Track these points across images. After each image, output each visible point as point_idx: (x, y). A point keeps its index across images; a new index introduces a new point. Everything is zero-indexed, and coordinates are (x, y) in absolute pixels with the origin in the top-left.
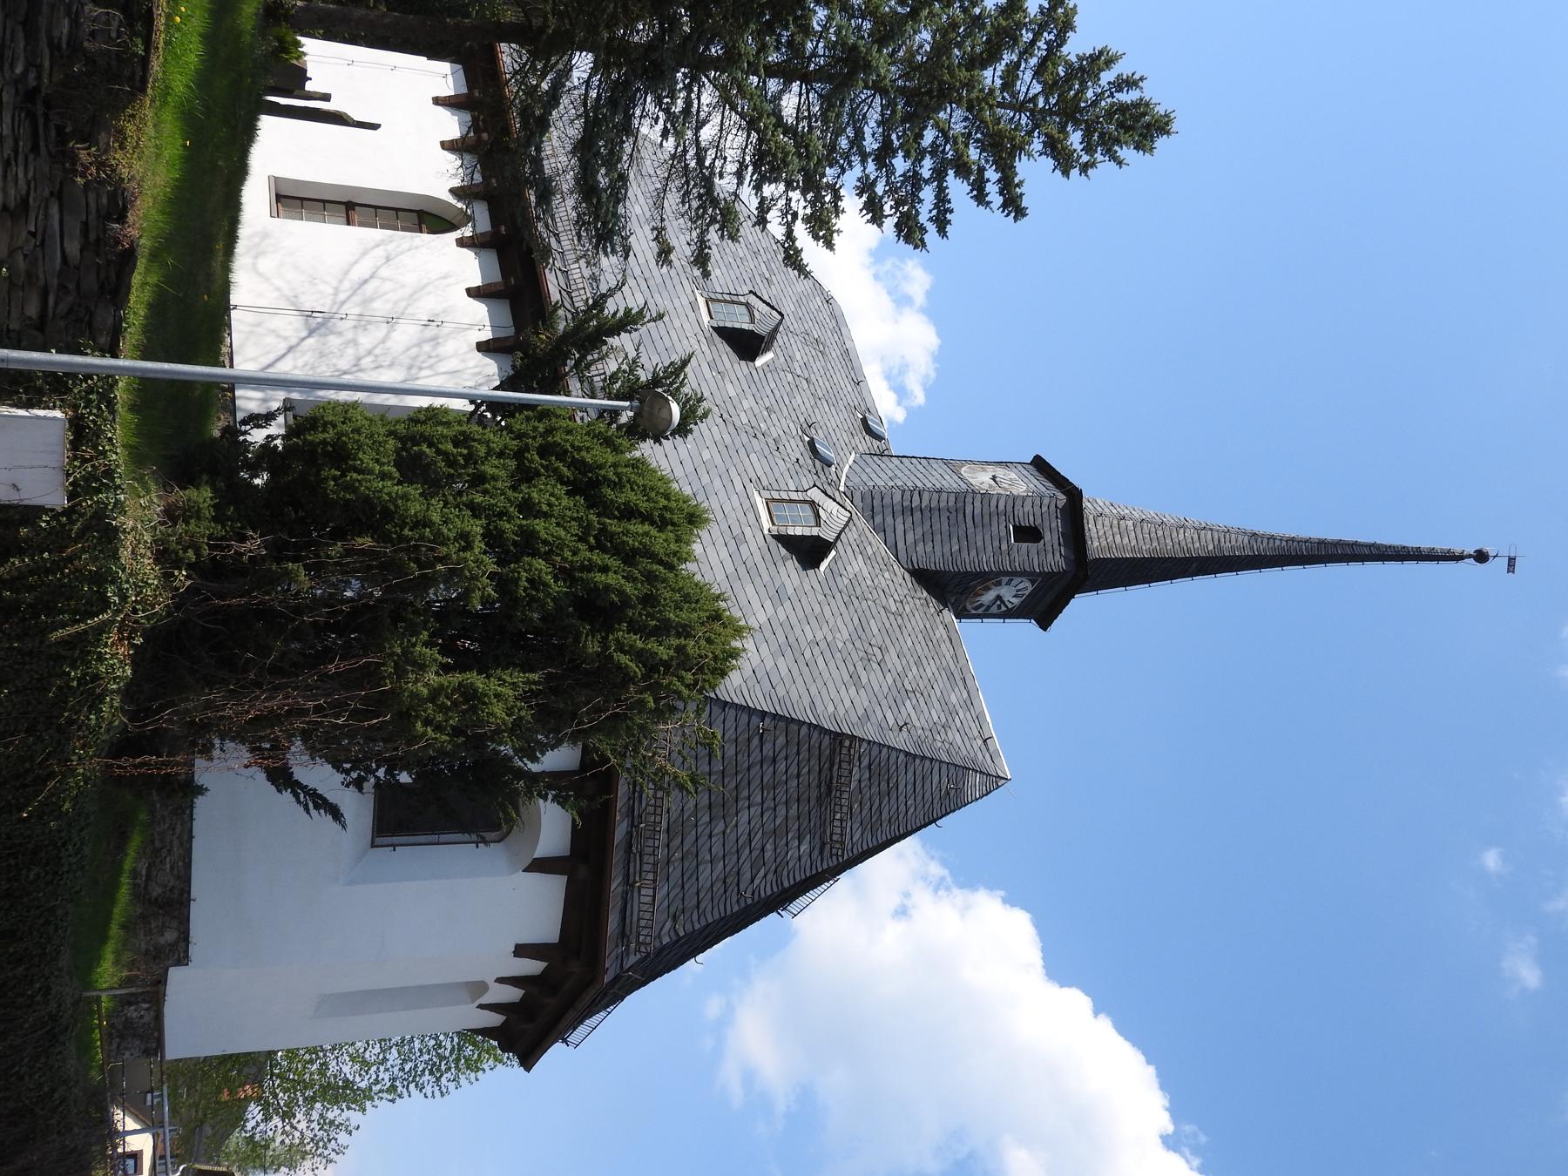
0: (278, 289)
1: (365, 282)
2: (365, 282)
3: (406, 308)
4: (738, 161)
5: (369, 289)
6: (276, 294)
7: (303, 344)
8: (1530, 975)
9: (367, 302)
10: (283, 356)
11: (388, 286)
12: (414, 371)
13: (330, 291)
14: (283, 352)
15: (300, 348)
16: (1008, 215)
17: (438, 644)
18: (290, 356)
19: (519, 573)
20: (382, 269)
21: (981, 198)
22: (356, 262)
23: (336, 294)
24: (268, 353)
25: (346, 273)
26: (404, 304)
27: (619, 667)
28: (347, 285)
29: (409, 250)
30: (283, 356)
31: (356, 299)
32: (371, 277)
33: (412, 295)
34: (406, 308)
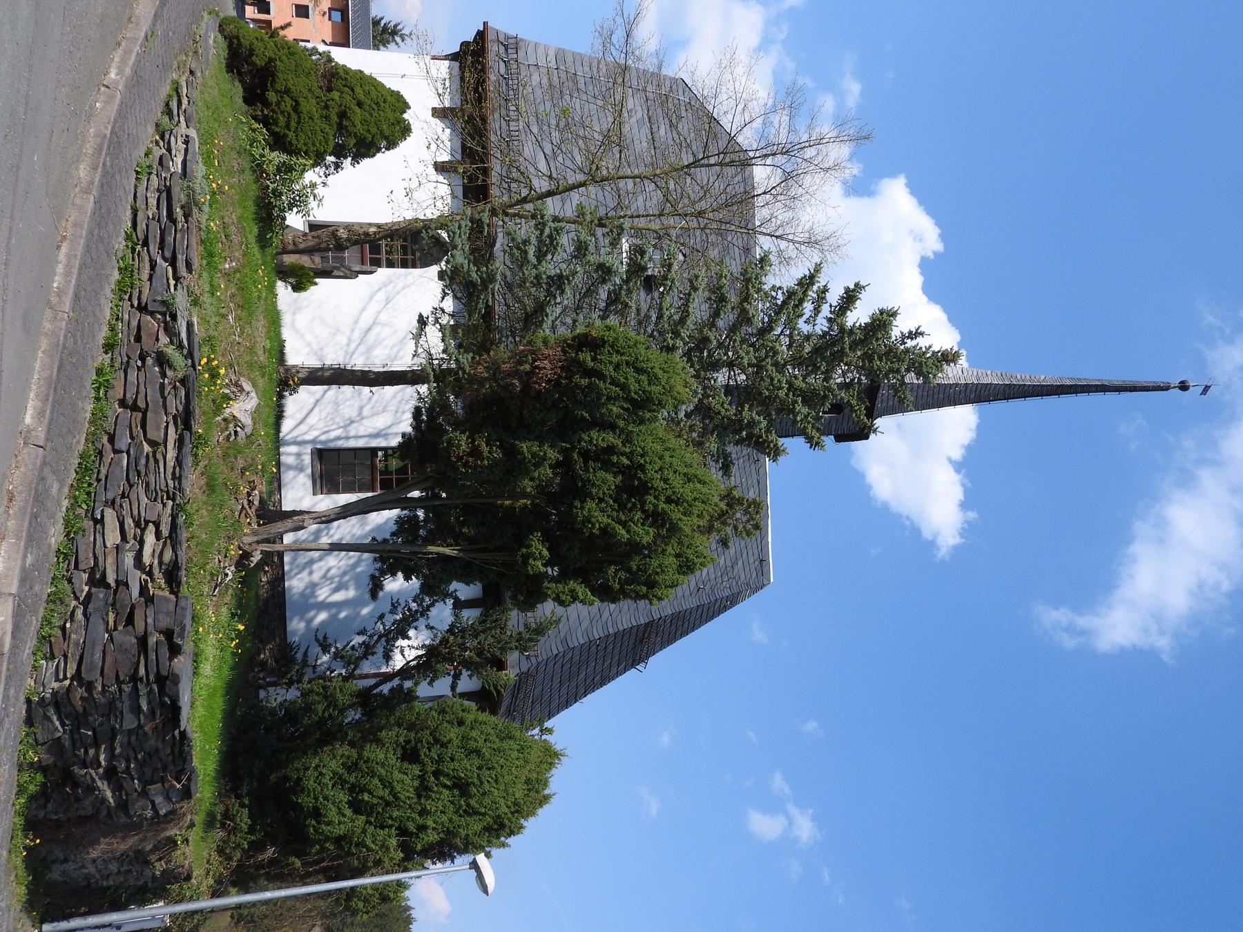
0: (309, 345)
1: (369, 329)
2: (369, 329)
3: (398, 352)
4: (419, 777)
5: (372, 337)
6: (307, 350)
7: (326, 396)
8: (811, 726)
9: (369, 350)
10: (311, 410)
11: (386, 331)
12: (399, 414)
13: (345, 341)
14: (311, 407)
15: (324, 401)
16: (850, 297)
17: (559, 473)
18: (316, 410)
19: (416, 844)
20: (381, 315)
21: (825, 290)
22: (363, 310)
23: (348, 345)
24: (302, 408)
25: (356, 322)
26: (396, 349)
27: (484, 228)
28: (357, 334)
29: (403, 289)
30: (311, 410)
31: (362, 348)
32: (374, 323)
33: (401, 341)
34: (398, 352)
